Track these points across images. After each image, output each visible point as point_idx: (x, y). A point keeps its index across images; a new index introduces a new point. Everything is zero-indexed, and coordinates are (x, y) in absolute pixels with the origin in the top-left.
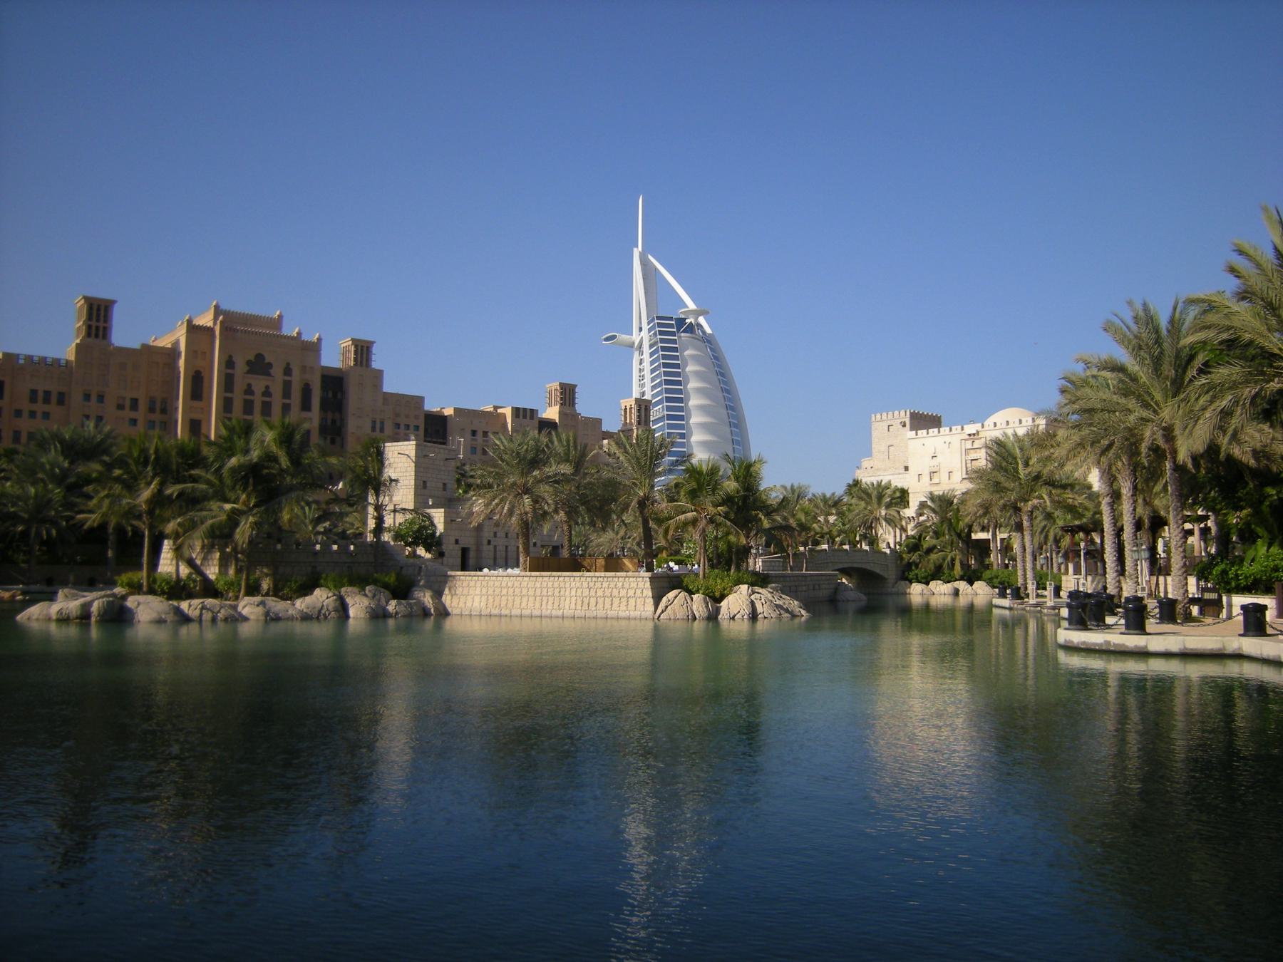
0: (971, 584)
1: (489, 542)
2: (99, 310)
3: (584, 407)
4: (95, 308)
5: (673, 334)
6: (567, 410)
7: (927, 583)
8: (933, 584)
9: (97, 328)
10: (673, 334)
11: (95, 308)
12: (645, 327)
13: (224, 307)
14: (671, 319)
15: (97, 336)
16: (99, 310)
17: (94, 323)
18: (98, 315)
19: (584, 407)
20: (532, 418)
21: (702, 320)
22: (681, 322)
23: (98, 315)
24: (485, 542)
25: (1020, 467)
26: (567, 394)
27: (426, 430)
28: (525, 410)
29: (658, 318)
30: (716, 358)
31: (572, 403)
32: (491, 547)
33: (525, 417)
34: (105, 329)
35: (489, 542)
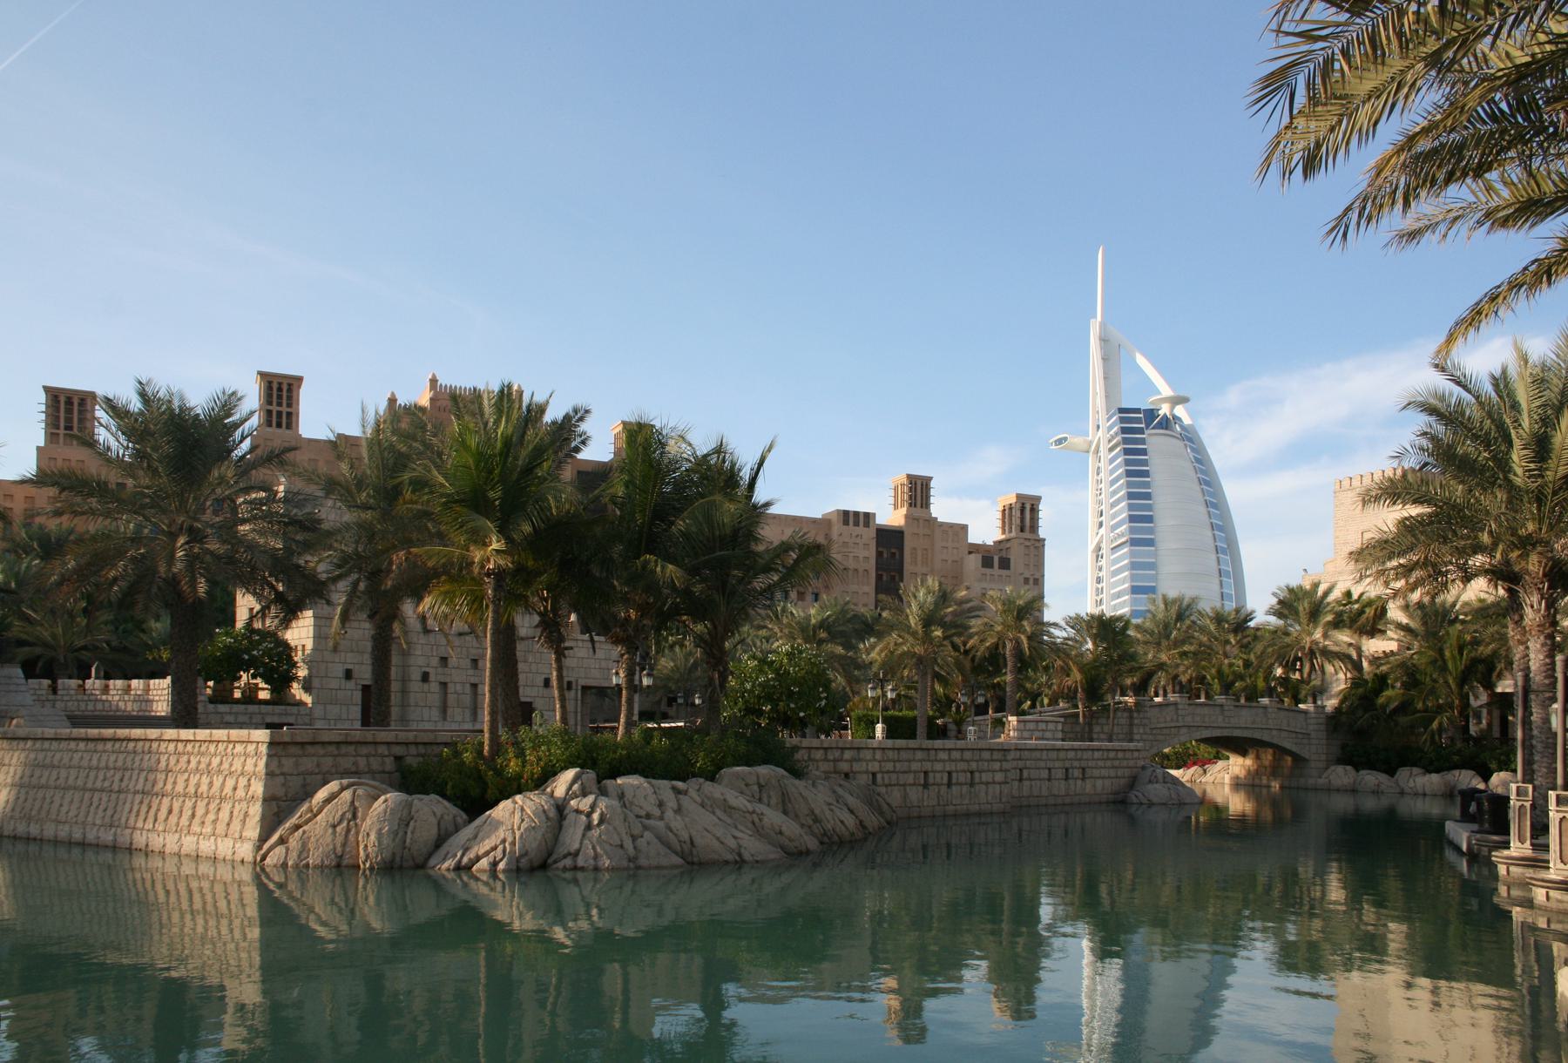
0: (1391, 772)
1: (425, 677)
2: (280, 389)
3: (942, 509)
4: (275, 386)
5: (1141, 431)
6: (918, 512)
7: (1391, 772)
8: (1403, 773)
9: (279, 414)
10: (1141, 431)
11: (275, 386)
12: (1104, 425)
13: (444, 380)
14: (1137, 411)
15: (279, 425)
16: (280, 389)
17: (275, 408)
18: (279, 397)
19: (942, 509)
20: (867, 524)
21: (1180, 411)
22: (1151, 414)
23: (279, 397)
24: (416, 675)
25: (1346, 68)
26: (918, 491)
27: (879, 577)
28: (856, 514)
29: (1121, 410)
30: (1198, 461)
31: (926, 504)
32: (434, 686)
33: (856, 524)
34: (289, 415)
35: (425, 677)
